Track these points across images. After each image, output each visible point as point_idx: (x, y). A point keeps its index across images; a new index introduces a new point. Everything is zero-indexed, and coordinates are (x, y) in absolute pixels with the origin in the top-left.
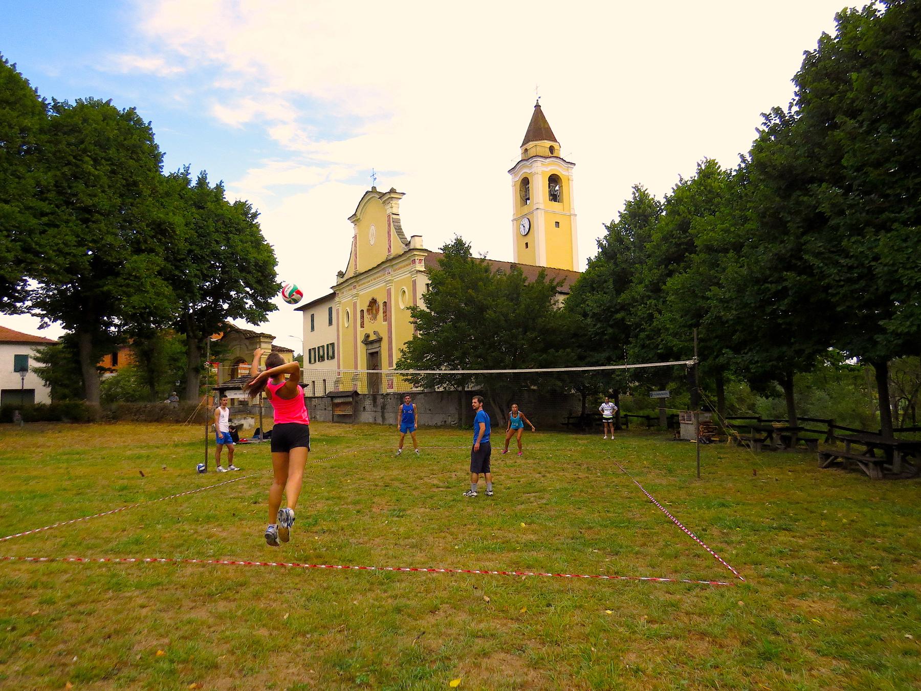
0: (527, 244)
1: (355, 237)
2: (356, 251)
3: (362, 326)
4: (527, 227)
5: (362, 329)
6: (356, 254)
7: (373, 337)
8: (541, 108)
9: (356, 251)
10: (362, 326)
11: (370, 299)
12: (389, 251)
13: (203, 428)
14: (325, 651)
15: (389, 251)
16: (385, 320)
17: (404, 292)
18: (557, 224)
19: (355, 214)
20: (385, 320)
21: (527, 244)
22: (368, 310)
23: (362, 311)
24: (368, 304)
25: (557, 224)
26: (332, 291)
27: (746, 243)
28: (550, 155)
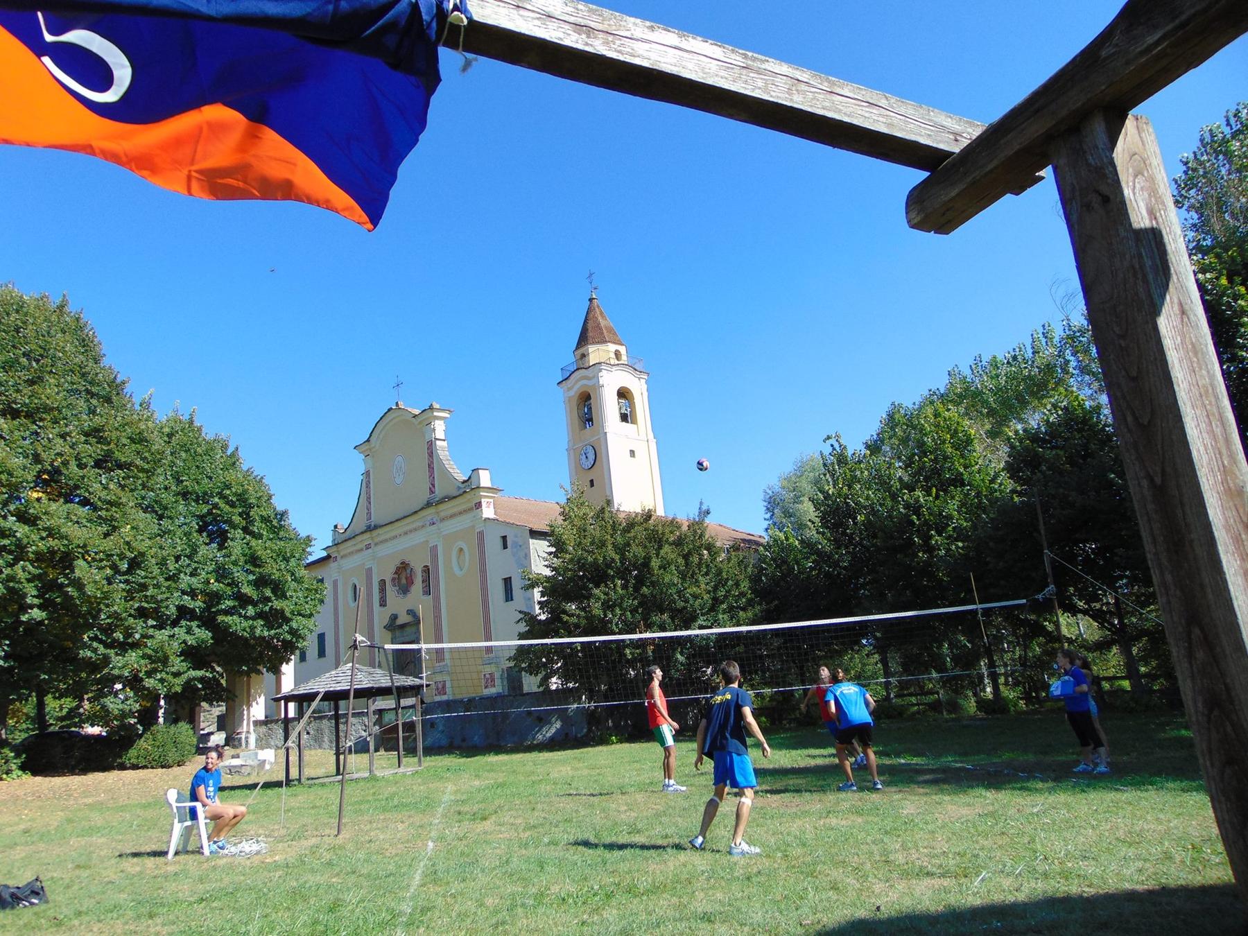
0: (592, 482)
1: (367, 474)
2: (368, 494)
3: (383, 603)
4: (591, 457)
5: (383, 609)
6: (369, 498)
7: (403, 619)
8: (1008, 197)
9: (368, 494)
10: (383, 603)
11: (398, 563)
12: (432, 492)
13: (204, 757)
14: (559, 928)
15: (432, 492)
16: (427, 592)
17: (461, 550)
18: (632, 453)
19: (368, 440)
20: (427, 592)
21: (592, 482)
22: (393, 579)
23: (383, 583)
24: (393, 569)
25: (632, 453)
26: (324, 554)
27: (892, 696)
28: (617, 362)
